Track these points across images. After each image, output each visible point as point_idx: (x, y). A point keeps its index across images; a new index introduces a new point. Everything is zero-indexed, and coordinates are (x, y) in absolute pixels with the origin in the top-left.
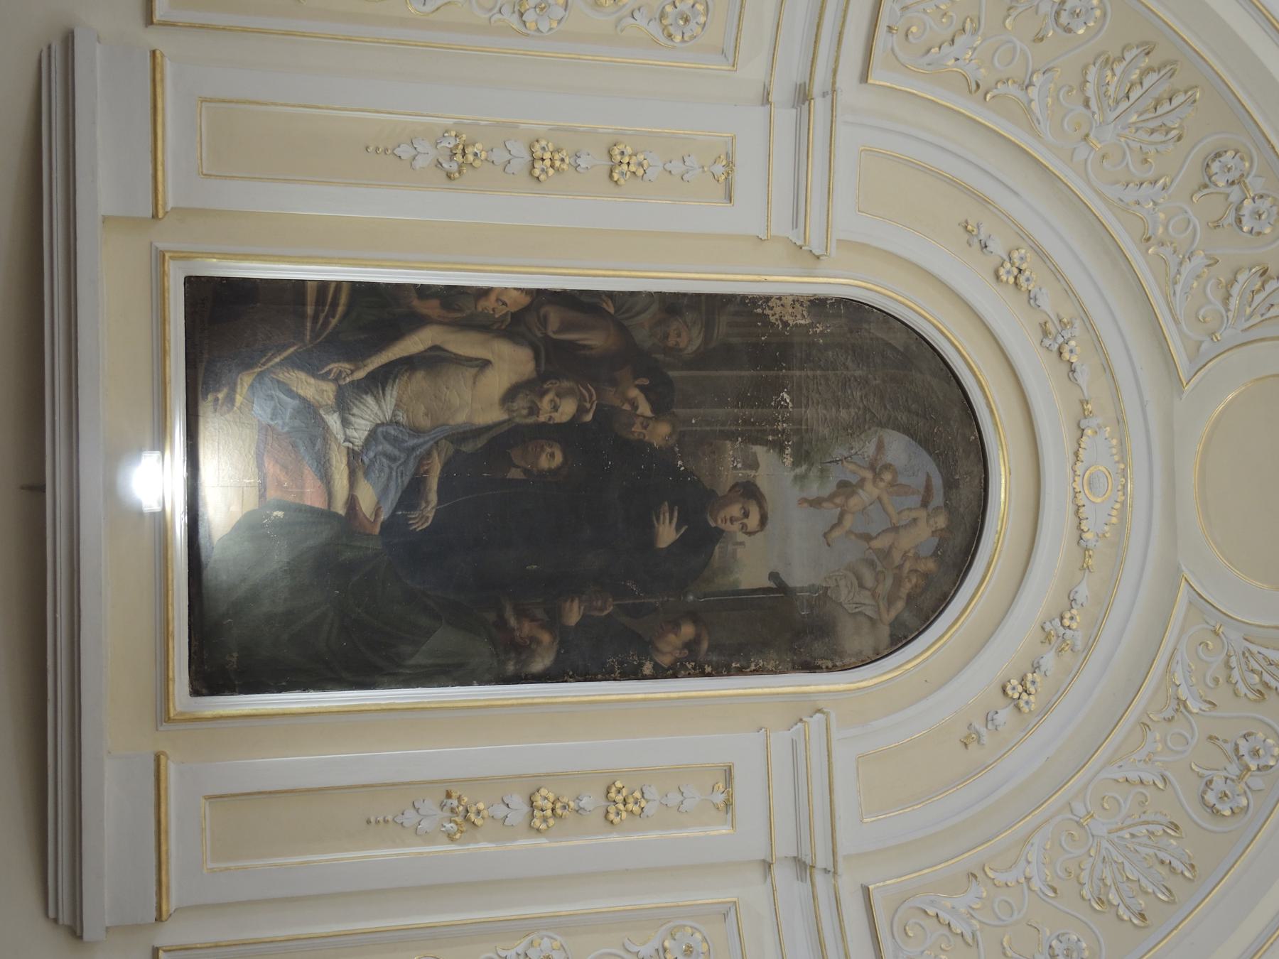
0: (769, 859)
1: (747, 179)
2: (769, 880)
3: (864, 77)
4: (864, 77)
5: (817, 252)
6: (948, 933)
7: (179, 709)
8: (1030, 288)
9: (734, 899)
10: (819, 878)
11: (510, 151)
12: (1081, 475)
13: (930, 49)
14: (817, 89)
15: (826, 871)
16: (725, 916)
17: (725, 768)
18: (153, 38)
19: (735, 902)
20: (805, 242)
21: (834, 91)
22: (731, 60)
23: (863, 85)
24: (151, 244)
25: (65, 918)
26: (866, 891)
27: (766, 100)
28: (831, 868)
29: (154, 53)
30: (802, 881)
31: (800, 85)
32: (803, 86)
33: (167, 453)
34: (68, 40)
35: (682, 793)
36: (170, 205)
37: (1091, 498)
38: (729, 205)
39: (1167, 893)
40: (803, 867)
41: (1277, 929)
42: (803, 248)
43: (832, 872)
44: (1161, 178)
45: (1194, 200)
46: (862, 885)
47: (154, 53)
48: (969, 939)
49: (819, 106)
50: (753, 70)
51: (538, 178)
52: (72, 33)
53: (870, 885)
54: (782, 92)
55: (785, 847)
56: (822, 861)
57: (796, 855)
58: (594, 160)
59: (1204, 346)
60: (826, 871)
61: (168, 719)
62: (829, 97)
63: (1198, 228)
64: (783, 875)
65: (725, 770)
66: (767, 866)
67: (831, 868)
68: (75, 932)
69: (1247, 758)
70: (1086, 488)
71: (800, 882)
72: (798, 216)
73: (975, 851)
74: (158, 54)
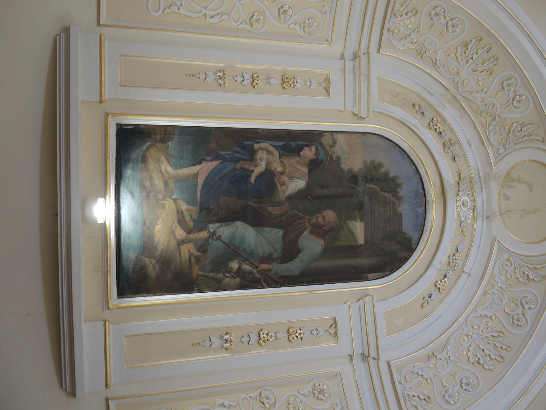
0: (352, 355)
1: (335, 87)
2: (352, 363)
3: (378, 51)
4: (378, 51)
5: (363, 116)
8: (440, 131)
10: (371, 361)
11: (243, 76)
12: (459, 200)
14: (361, 52)
15: (374, 358)
16: (336, 376)
18: (102, 30)
20: (359, 113)
21: (368, 53)
22: (330, 43)
23: (378, 54)
25: (64, 388)
26: (388, 363)
27: (342, 58)
29: (100, 36)
30: (364, 362)
33: (107, 197)
34: (67, 31)
36: (107, 97)
37: (463, 208)
38: (329, 98)
39: (500, 358)
40: (365, 357)
42: (358, 115)
43: (377, 359)
44: (484, 88)
45: (497, 98)
46: (387, 361)
47: (100, 36)
49: (363, 58)
50: (338, 48)
51: (254, 86)
52: (69, 27)
54: (348, 55)
55: (358, 350)
56: (373, 354)
57: (362, 352)
58: (276, 81)
59: (500, 151)
60: (374, 358)
62: (367, 55)
64: (357, 359)
66: (351, 356)
67: (376, 357)
68: (73, 393)
69: (525, 305)
70: (461, 205)
71: (364, 363)
72: (356, 101)
74: (102, 37)
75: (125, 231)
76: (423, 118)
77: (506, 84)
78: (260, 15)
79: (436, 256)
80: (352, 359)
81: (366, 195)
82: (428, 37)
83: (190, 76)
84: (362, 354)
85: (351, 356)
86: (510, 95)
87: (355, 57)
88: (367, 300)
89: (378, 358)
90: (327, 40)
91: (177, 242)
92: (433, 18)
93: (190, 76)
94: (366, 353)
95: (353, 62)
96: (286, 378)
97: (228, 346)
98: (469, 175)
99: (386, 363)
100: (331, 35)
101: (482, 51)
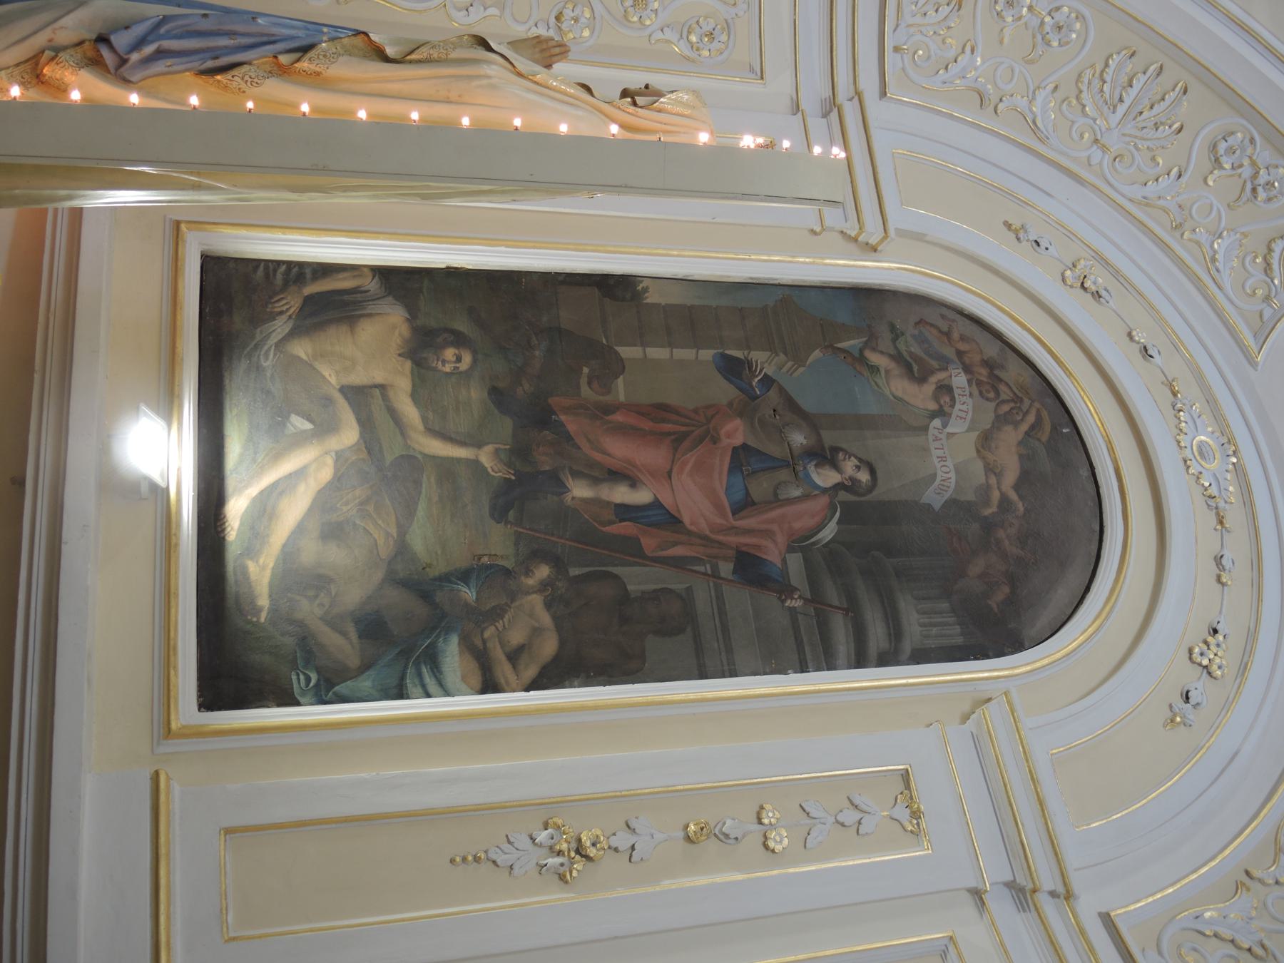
3: (883, 94)
4: (883, 94)
6: (1233, 951)
7: (183, 722)
9: (950, 934)
10: (1049, 908)
13: (939, 71)
15: (1053, 894)
16: (944, 954)
17: (901, 772)
19: (951, 938)
22: (759, 73)
24: (165, 217)
26: (1107, 921)
28: (1061, 889)
30: (1024, 911)
31: (825, 99)
32: (828, 100)
35: (808, 814)
40: (1022, 894)
41: (1215, 6)
43: (1067, 895)
45: (1211, 183)
48: (1260, 951)
53: (1112, 911)
54: (812, 98)
55: (994, 871)
56: (1048, 880)
57: (1009, 878)
60: (1053, 894)
61: (168, 733)
62: (856, 99)
63: (1222, 210)
64: (1002, 906)
65: (902, 775)
67: (1061, 889)
73: (1186, 881)
75: (235, 574)
76: (1036, 252)
77: (1226, 150)
78: (580, 6)
79: (1163, 587)
80: (983, 903)
81: (948, 605)
82: (1002, 63)
83: (464, 859)
84: (1011, 885)
85: (977, 894)
86: (1243, 176)
87: (831, 106)
88: (994, 714)
89: (1068, 891)
90: (752, 70)
91: (393, 579)
92: (1004, 13)
93: (464, 859)
94: (1022, 880)
95: (825, 120)
96: (680, 71)
97: (562, 865)
98: (1156, 78)
99: (1097, 916)
100: (758, 39)
101: (1143, 78)
